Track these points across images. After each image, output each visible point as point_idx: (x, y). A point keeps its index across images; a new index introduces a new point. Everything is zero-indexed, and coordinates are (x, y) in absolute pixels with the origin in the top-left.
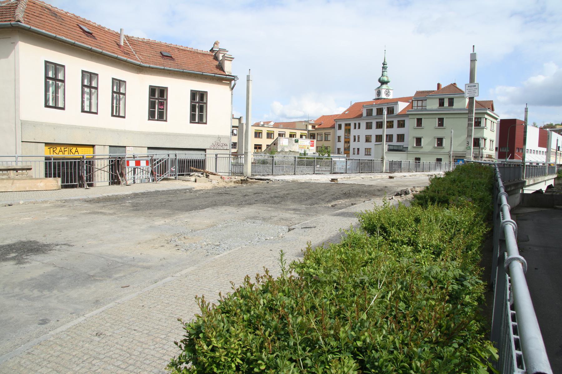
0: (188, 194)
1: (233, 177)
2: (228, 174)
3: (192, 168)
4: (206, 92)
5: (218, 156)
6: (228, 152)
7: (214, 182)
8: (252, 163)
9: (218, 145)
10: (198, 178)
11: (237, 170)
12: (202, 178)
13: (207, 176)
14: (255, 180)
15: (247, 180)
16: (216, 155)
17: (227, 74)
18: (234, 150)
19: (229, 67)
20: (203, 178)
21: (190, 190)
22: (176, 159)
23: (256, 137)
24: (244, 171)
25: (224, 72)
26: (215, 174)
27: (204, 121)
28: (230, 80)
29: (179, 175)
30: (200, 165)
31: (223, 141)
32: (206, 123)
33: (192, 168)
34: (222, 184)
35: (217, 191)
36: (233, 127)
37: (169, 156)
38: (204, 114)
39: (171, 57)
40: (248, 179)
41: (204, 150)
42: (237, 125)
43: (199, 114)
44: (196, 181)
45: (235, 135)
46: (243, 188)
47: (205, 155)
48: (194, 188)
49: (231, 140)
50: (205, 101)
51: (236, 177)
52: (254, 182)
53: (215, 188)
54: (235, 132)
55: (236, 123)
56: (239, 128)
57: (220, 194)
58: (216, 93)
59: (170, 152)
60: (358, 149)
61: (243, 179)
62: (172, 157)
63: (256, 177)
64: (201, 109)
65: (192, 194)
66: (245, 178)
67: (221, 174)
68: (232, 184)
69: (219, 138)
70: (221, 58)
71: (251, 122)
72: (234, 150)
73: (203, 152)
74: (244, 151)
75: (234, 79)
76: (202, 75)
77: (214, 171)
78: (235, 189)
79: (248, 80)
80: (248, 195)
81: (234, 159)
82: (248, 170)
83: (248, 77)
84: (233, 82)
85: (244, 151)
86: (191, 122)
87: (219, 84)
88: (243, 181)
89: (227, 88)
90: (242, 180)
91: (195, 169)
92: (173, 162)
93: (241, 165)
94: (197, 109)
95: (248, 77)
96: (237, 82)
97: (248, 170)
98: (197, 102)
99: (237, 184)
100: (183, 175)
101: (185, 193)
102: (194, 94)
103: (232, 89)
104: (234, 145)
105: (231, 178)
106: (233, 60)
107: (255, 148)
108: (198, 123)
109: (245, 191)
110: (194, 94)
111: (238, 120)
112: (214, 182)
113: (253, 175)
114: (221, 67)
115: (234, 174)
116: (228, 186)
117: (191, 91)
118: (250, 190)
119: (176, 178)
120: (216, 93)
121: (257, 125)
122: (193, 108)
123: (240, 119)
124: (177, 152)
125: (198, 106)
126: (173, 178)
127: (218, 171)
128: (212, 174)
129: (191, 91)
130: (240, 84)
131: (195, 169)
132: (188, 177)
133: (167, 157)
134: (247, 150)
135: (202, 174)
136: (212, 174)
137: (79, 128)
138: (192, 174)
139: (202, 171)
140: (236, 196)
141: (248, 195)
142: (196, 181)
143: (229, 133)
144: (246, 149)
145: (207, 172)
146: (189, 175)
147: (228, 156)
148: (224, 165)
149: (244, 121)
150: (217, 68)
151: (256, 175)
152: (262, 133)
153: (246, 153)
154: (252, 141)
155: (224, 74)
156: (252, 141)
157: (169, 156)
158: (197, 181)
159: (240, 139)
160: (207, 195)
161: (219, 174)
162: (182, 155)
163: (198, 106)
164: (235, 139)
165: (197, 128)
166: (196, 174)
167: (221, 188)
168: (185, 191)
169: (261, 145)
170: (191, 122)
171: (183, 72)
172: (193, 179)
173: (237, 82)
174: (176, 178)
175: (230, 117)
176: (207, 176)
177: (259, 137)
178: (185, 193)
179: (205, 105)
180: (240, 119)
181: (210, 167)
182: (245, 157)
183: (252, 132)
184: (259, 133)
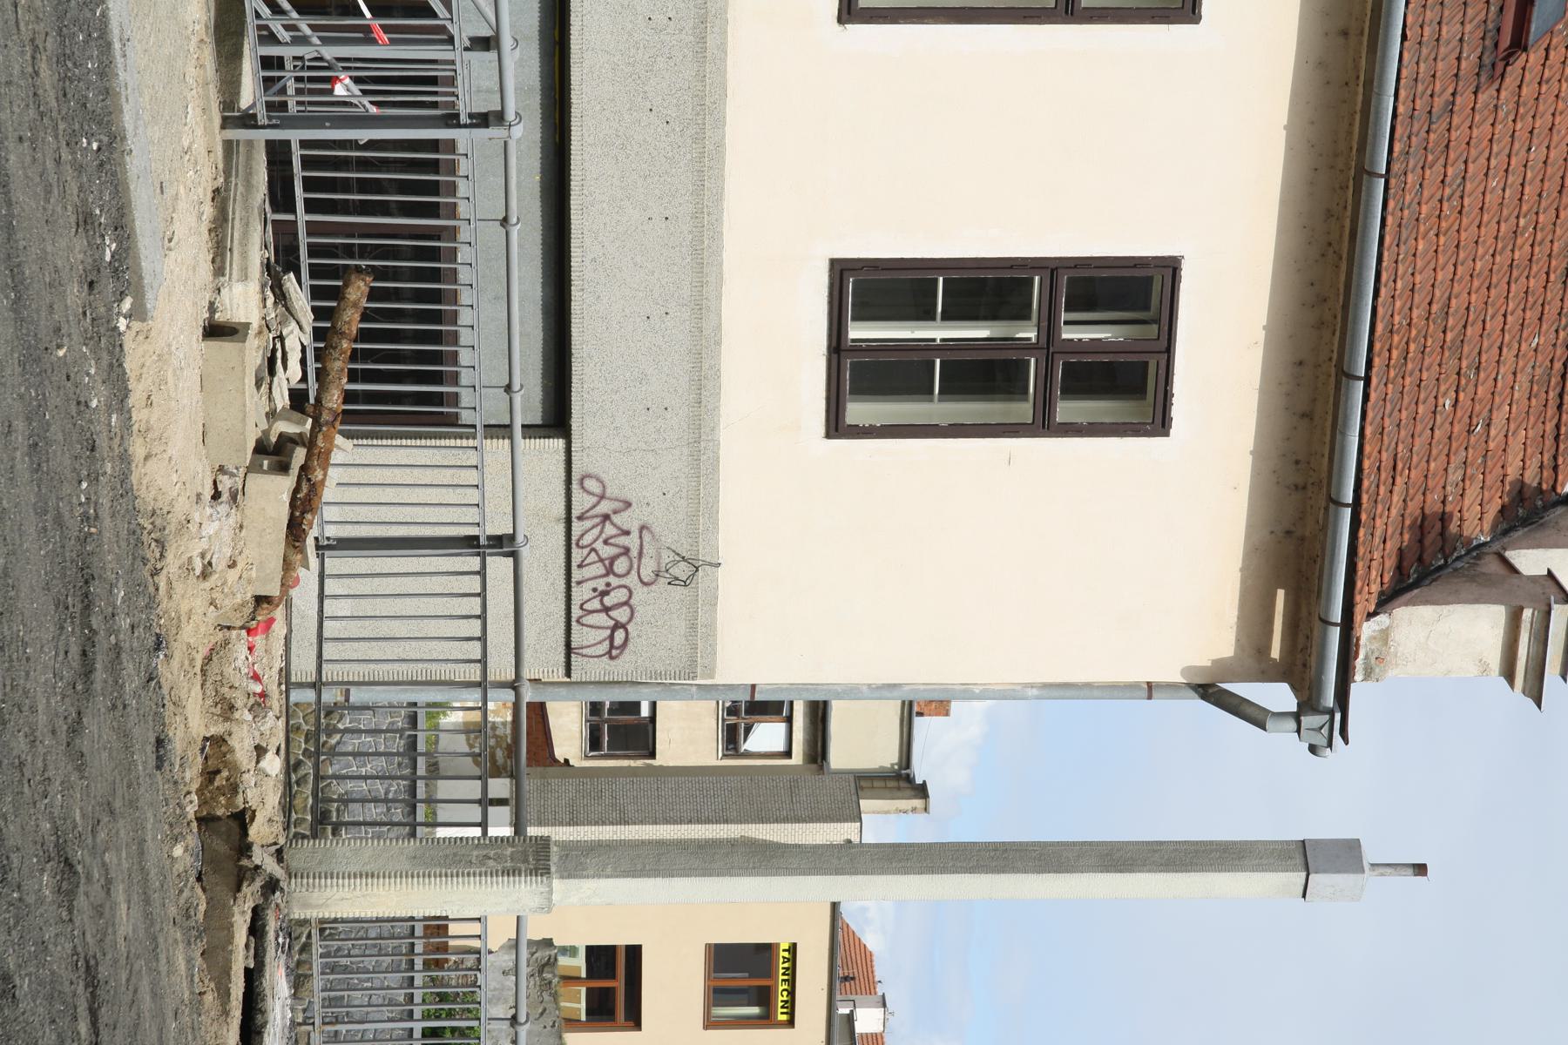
0: (70, 250)
1: (273, 728)
2: (304, 667)
3: (358, 291)
4: (1160, 424)
5: (499, 566)
6: (543, 660)
7: (213, 539)
8: (437, 927)
9: (623, 561)
10: (253, 351)
11: (360, 772)
12: (255, 404)
13: (273, 453)
14: (240, 960)
15: (240, 878)
16: (504, 544)
17: (1367, 631)
18: (568, 731)
19: (1437, 647)
20: (252, 413)
21: (116, 275)
22: (452, 120)
23: (724, 958)
24: (345, 849)
25: (1386, 600)
26: (295, 531)
27: (858, 411)
28: (1298, 669)
29: (278, 155)
30: (391, 368)
31: (655, 610)
32: (836, 427)
33: (358, 291)
34: (192, 615)
35: (110, 560)
36: (819, 714)
37: (484, 44)
38: (937, 410)
39: (1519, 43)
40: (250, 894)
41: (557, 418)
42: (841, 756)
43: (927, 346)
44: (216, 331)
45: (732, 739)
46: (154, 836)
47: (501, 430)
48: (138, 313)
49: (671, 690)
50: (1065, 410)
51: (273, 764)
52: (216, 957)
53: (145, 539)
54: (766, 736)
55: (860, 742)
56: (802, 772)
57: (81, 589)
58: (1146, 530)
59: (521, 63)
60: (793, 949)
61: (259, 831)
62: (475, 81)
63: (278, 983)
64: (982, 377)
65: (74, 293)
66: (261, 857)
67: (304, 595)
68: (192, 721)
69: (690, 570)
70: (1530, 561)
71: (879, 908)
72: (568, 731)
73: (529, 404)
74: (560, 834)
75: (1308, 703)
76: (1344, 375)
77: (331, 520)
78: (144, 757)
79: (1305, 857)
80: (67, 895)
81: (479, 730)
82: (361, 891)
83: (1346, 856)
84: (1279, 696)
85: (560, 834)
86: (841, 270)
87: (1252, 551)
88: (227, 831)
89: (1213, 637)
90: (242, 819)
91: (351, 320)
92: (421, 89)
93: (411, 814)
94: (978, 331)
95: (1344, 855)
96: (1284, 743)
97: (361, 891)
98: (1049, 329)
99: (192, 775)
100: (281, 196)
101: (85, 221)
102: (1139, 292)
103: (1208, 691)
104: (621, 729)
105: (259, 704)
106: (1516, 698)
107: (600, 957)
108: (837, 345)
109: (119, 861)
110: (1139, 292)
111: (887, 757)
112: (212, 531)
113: (291, 929)
114: (1432, 562)
115: (315, 734)
116: (176, 672)
117: (1171, 268)
118: (126, 919)
119: (247, 121)
120: (1146, 530)
121: (850, 971)
122: (988, 287)
123: (901, 781)
124: (525, 135)
125: (1033, 344)
126: (249, 94)
127: (334, 564)
128: (303, 505)
129: (1171, 268)
130: (1260, 776)
131: (351, 320)
132: (254, 249)
133: (466, 27)
134: (569, 873)
135: (298, 399)
136: (303, 505)
137: (699, 187)
138: (301, 299)
139: (334, 400)
140: (60, 768)
141: (67, 895)
142: (216, 331)
143: (746, 662)
144: (580, 861)
145: (318, 456)
146: (283, 258)
147: (501, 667)
148: (394, 631)
149: (882, 822)
150: (1421, 527)
151: (298, 981)
152: (765, 1020)
153: (534, 860)
154: (674, 922)
155: (1359, 611)
156: (674, 922)
157: (484, 44)
158: (223, 348)
159: (695, 792)
160: (61, 459)
161: (307, 578)
162: (492, 183)
163: (1033, 344)
164: (688, 735)
165: (778, 340)
166: (297, 338)
167: (146, 597)
168: (106, 217)
169: (634, 1020)
170: (841, 270)
171: (1364, 173)
172: (244, 300)
173: (1284, 745)
174: (247, 121)
175: (920, 674)
176: (273, 453)
177: (718, 994)
178: (85, 221)
179: (1023, 410)
180: (901, 781)
181: (370, 478)
182: (487, 842)
183: (776, 911)
184: (763, 997)
